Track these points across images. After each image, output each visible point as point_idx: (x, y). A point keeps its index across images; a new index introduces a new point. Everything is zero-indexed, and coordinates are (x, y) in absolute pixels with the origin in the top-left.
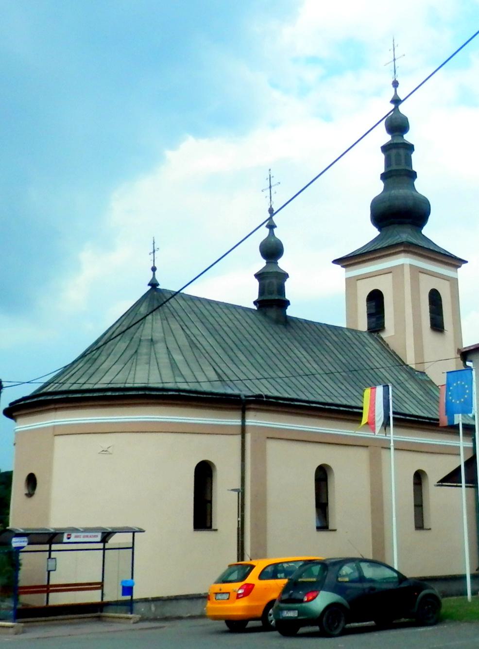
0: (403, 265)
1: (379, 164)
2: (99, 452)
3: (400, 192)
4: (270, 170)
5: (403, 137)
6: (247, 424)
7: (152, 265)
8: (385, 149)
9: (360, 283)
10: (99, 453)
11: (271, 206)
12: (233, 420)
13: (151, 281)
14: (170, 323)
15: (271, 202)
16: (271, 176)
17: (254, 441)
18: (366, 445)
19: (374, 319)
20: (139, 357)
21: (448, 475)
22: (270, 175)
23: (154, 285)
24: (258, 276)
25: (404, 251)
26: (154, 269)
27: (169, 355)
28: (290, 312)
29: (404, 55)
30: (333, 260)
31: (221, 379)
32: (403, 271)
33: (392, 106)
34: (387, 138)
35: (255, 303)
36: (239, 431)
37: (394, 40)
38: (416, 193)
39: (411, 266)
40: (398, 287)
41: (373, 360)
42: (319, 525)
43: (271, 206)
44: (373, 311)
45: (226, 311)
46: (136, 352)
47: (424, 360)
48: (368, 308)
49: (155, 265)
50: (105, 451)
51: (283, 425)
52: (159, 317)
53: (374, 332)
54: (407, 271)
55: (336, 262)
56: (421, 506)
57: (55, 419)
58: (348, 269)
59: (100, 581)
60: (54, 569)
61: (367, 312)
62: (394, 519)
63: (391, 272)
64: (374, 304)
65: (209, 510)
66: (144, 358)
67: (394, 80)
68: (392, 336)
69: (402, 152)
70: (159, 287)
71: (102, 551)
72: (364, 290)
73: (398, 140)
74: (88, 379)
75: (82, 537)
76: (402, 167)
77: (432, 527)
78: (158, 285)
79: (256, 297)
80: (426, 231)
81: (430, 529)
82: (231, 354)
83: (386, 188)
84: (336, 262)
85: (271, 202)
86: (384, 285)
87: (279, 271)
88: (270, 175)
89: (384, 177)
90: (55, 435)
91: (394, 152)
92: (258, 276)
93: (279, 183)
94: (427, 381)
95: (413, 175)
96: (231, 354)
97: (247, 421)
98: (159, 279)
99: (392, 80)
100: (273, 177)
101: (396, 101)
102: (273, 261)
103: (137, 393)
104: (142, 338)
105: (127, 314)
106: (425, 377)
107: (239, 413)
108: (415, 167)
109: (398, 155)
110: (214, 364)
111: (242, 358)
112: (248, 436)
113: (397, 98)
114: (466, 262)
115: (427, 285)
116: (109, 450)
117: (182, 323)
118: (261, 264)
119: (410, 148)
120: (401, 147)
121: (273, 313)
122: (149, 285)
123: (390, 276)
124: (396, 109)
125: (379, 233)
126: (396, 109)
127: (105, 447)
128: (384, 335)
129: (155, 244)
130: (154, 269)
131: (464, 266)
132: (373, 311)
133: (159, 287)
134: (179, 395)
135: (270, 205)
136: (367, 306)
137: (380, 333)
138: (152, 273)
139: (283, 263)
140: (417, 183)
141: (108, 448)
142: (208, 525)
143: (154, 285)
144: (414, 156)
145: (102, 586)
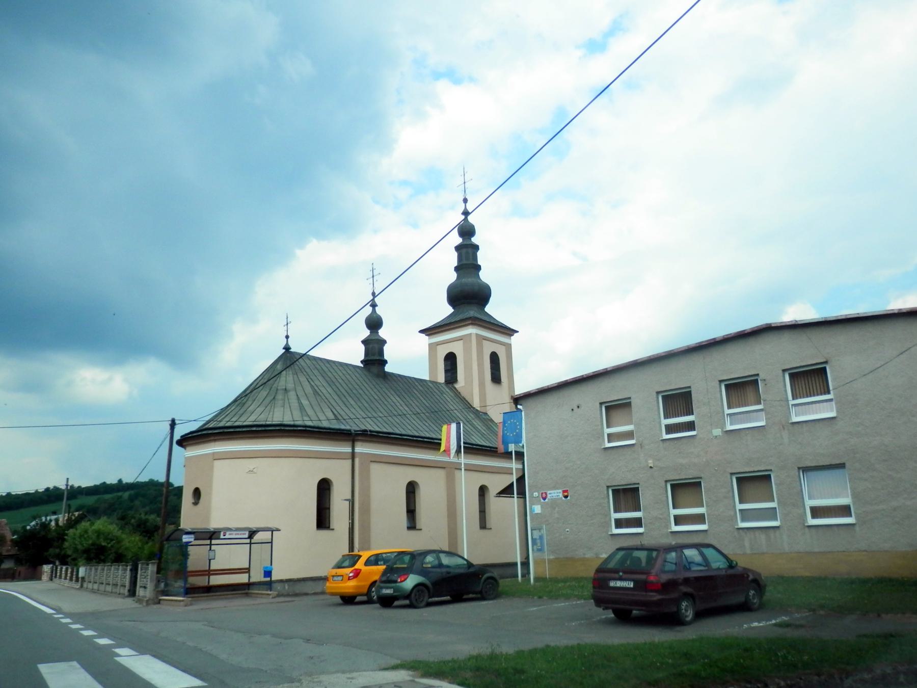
0: (471, 334)
7: (286, 334)
12: (346, 449)
14: (299, 377)
19: (449, 374)
23: (287, 348)
24: (364, 342)
25: (472, 324)
26: (287, 337)
28: (388, 368)
29: (472, 179)
33: (463, 217)
36: (350, 456)
38: (480, 281)
44: (449, 368)
46: (274, 398)
48: (446, 366)
53: (450, 383)
55: (422, 331)
59: (248, 567)
63: (462, 339)
66: (280, 402)
69: (470, 250)
70: (291, 350)
71: (249, 545)
72: (442, 352)
76: (471, 262)
77: (492, 528)
78: (290, 349)
79: (362, 357)
80: (488, 309)
81: (491, 529)
82: (344, 399)
84: (422, 331)
89: (457, 269)
90: (215, 460)
91: (464, 251)
92: (364, 342)
95: (478, 268)
96: (344, 399)
99: (462, 198)
101: (466, 213)
107: (350, 443)
108: (479, 263)
109: (467, 253)
111: (352, 402)
112: (357, 460)
115: (488, 348)
119: (476, 248)
121: (375, 369)
122: (284, 348)
124: (466, 219)
125: (453, 310)
127: (251, 468)
130: (287, 337)
131: (515, 334)
132: (449, 368)
133: (291, 350)
136: (444, 364)
138: (286, 340)
139: (382, 333)
141: (254, 469)
142: (327, 526)
143: (287, 348)
144: (479, 254)
145: (249, 570)
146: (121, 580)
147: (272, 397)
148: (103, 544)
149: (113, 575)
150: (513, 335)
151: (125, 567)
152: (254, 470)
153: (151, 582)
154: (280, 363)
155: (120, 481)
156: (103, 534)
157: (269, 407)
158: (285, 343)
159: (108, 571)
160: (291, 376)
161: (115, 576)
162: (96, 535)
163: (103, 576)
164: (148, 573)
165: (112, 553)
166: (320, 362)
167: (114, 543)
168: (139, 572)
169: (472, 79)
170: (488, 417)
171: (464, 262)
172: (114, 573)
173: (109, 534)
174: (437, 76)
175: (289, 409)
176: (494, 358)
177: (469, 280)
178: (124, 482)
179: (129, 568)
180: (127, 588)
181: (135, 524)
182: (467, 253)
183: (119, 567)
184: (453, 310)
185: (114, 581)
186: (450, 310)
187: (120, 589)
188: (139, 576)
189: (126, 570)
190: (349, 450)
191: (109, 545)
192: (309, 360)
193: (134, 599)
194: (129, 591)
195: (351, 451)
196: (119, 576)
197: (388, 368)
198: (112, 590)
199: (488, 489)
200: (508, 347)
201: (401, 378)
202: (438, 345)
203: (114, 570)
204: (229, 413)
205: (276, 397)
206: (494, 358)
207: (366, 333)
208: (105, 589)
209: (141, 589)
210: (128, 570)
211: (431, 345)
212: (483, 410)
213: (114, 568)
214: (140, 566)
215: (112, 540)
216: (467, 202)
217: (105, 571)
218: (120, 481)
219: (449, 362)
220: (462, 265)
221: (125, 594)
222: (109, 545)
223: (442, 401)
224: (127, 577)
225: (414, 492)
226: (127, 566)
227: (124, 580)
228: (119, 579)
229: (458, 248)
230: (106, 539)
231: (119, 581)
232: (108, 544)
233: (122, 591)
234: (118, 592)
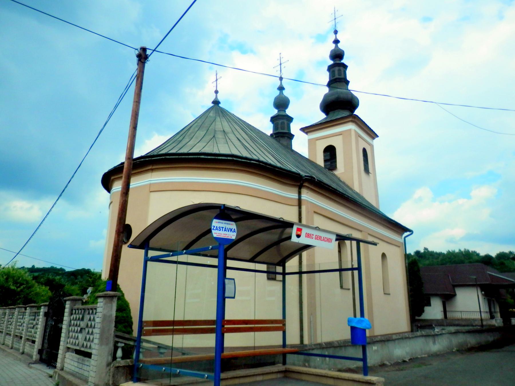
0: (350, 130)
1: (326, 78)
3: (340, 91)
5: (285, 111)
6: (302, 198)
7: (215, 89)
9: (318, 142)
12: (292, 194)
13: (215, 99)
15: (281, 73)
17: (308, 212)
18: (361, 229)
19: (329, 163)
22: (280, 57)
23: (216, 102)
25: (352, 121)
26: (216, 92)
29: (342, 15)
30: (300, 128)
32: (351, 133)
34: (275, 112)
36: (296, 203)
37: (335, 8)
39: (355, 131)
40: (347, 143)
44: (328, 158)
46: (214, 136)
48: (325, 156)
49: (218, 89)
51: (321, 204)
54: (353, 133)
57: (151, 178)
59: (280, 317)
60: (233, 296)
61: (324, 159)
62: (493, 274)
63: (341, 134)
64: (329, 154)
67: (335, 29)
68: (342, 173)
70: (220, 105)
71: (297, 276)
72: (322, 146)
73: (282, 113)
74: (179, 150)
75: (314, 237)
76: (342, 76)
77: (391, 293)
81: (389, 294)
83: (330, 91)
85: (281, 73)
86: (337, 143)
88: (280, 57)
90: (151, 192)
95: (347, 82)
97: (302, 195)
98: (220, 98)
99: (333, 31)
100: (283, 58)
101: (336, 42)
102: (283, 109)
103: (226, 158)
104: (216, 130)
105: (199, 118)
107: (296, 190)
109: (339, 70)
112: (304, 208)
113: (337, 39)
115: (362, 145)
120: (341, 66)
123: (341, 137)
124: (337, 46)
126: (337, 46)
128: (336, 173)
129: (217, 75)
130: (216, 92)
132: (328, 158)
134: (259, 164)
136: (323, 155)
138: (215, 94)
139: (289, 112)
140: (350, 87)
143: (216, 102)
144: (348, 72)
145: (284, 325)
146: (27, 331)
147: (212, 136)
148: (13, 287)
149: (17, 322)
151: (35, 310)
153: (101, 343)
154: (212, 112)
155: (33, 266)
156: (13, 277)
159: (11, 317)
161: (18, 324)
162: (5, 277)
163: (3, 323)
164: (38, 320)
165: (20, 298)
167: (24, 288)
168: (66, 318)
169: (252, 51)
172: (17, 319)
173: (19, 279)
174: (232, 48)
176: (364, 151)
178: (36, 267)
179: (43, 310)
180: (38, 345)
181: (44, 282)
182: (339, 70)
183: (26, 309)
185: (17, 331)
187: (24, 345)
188: (64, 326)
189: (36, 314)
190: (295, 196)
191: (19, 289)
193: (51, 371)
194: (40, 352)
195: (297, 197)
196: (25, 325)
198: (12, 343)
200: (372, 146)
202: (317, 140)
203: (18, 315)
204: (165, 148)
206: (364, 151)
208: (4, 340)
209: (69, 355)
210: (41, 314)
211: (310, 141)
213: (19, 312)
214: (68, 305)
215: (22, 284)
217: (7, 316)
218: (33, 266)
221: (31, 356)
222: (19, 289)
224: (39, 326)
226: (39, 308)
227: (33, 331)
228: (25, 328)
230: (15, 282)
231: (24, 333)
232: (18, 287)
233: (27, 349)
234: (21, 351)
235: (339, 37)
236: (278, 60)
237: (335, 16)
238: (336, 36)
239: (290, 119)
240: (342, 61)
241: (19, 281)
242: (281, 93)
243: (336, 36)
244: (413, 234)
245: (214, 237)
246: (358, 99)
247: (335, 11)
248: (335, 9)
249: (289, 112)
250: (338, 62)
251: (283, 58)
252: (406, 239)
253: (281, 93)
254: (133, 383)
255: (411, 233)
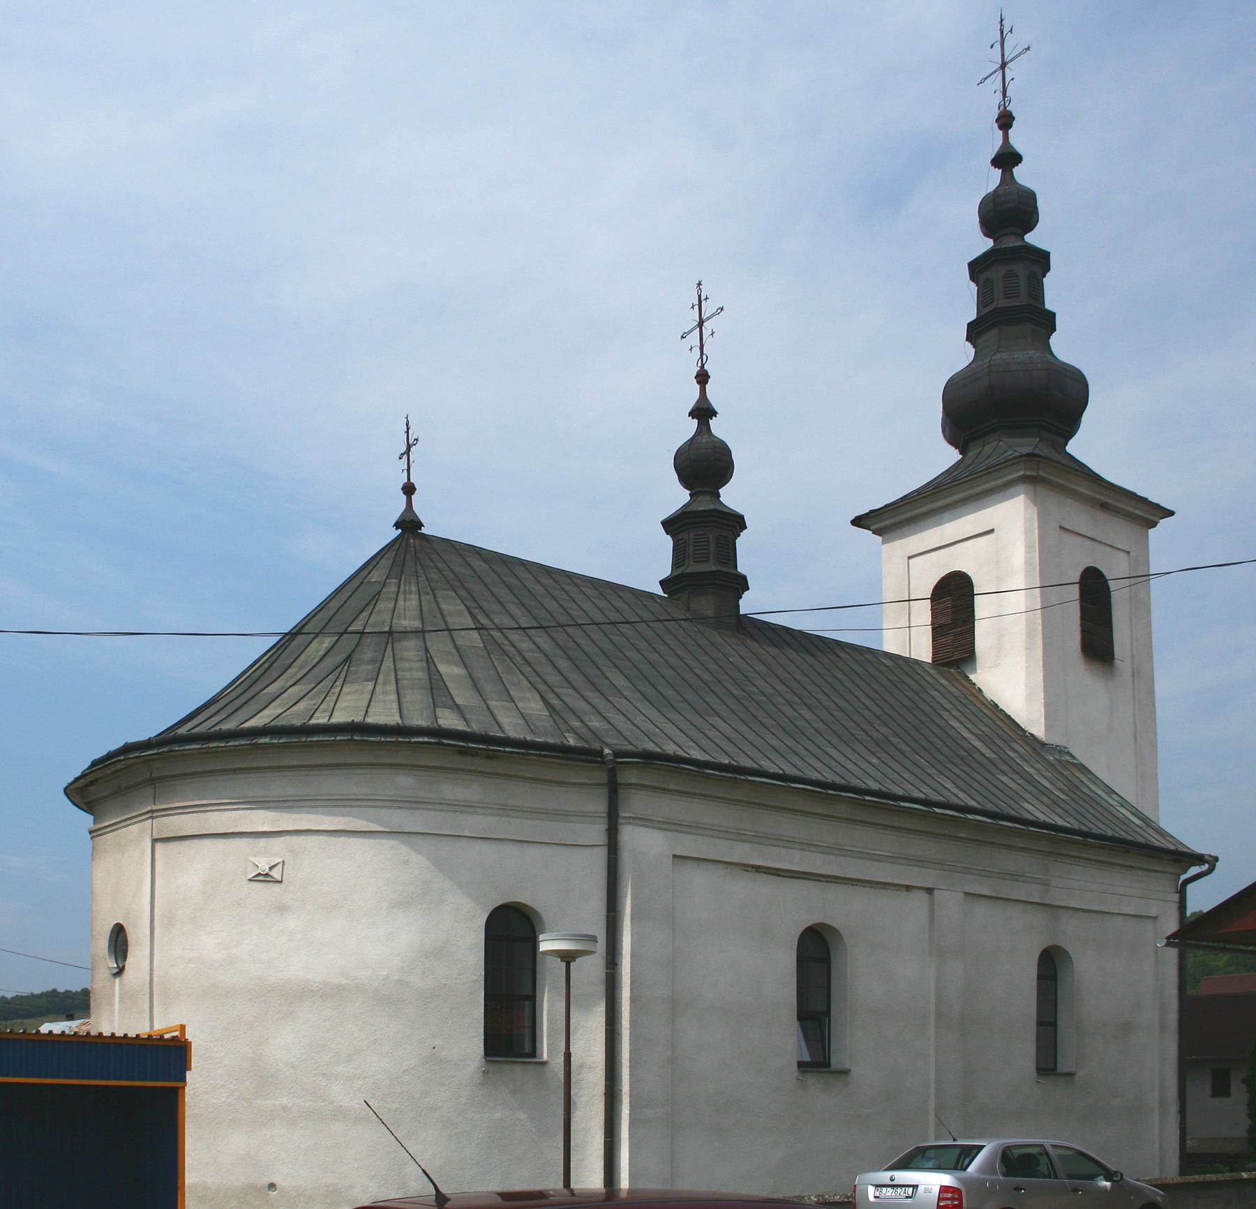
2: (251, 876)
4: (699, 284)
5: (1024, 239)
8: (977, 268)
10: (250, 880)
11: (703, 366)
14: (440, 600)
16: (703, 297)
20: (352, 669)
21: (1217, 907)
23: (409, 524)
24: (670, 525)
27: (428, 663)
28: (748, 604)
29: (1028, 49)
31: (478, 626)
33: (997, 174)
35: (663, 583)
37: (1002, 20)
38: (1049, 357)
41: (946, 715)
42: (807, 1058)
43: (703, 366)
44: (946, 620)
45: (589, 592)
47: (1149, 572)
50: (264, 878)
52: (414, 588)
53: (949, 664)
55: (858, 522)
56: (1054, 1025)
58: (886, 536)
65: (527, 1021)
66: (365, 669)
69: (1020, 269)
70: (424, 530)
78: (420, 525)
79: (666, 571)
80: (1073, 447)
82: (591, 671)
84: (858, 522)
87: (720, 508)
89: (975, 332)
91: (997, 273)
92: (670, 525)
93: (722, 309)
94: (1072, 764)
95: (1047, 322)
96: (591, 671)
99: (995, 113)
106: (1068, 758)
110: (542, 687)
111: (620, 682)
114: (1171, 513)
116: (276, 874)
117: (470, 603)
118: (678, 497)
119: (1041, 260)
121: (706, 605)
122: (397, 525)
125: (1001, 170)
126: (1007, 177)
127: (264, 867)
131: (1163, 523)
133: (424, 530)
135: (700, 364)
137: (963, 668)
139: (730, 496)
140: (1054, 341)
141: (271, 868)
142: (527, 1049)
143: (409, 524)
144: (1050, 283)
147: (345, 656)
150: (1154, 525)
152: (272, 873)
157: (327, 683)
158: (403, 506)
160: (415, 596)
166: (520, 572)
170: (1068, 758)
171: (1002, 303)
175: (392, 687)
177: (1021, 355)
184: (1001, 170)
186: (952, 456)
192: (485, 561)
197: (748, 604)
199: (1072, 962)
201: (792, 636)
205: (356, 656)
207: (678, 497)
212: (1056, 740)
216: (1010, 126)
219: (949, 603)
220: (997, 312)
223: (922, 706)
225: (826, 961)
229: (977, 268)
235: (1017, 139)
236: (693, 307)
237: (1003, 55)
238: (1006, 137)
239: (737, 523)
240: (1031, 238)
241: (548, 714)
242: (704, 428)
243: (1006, 137)
244: (1214, 873)
245: (92, 815)
246: (1087, 386)
247: (1002, 32)
248: (1002, 25)
249: (730, 496)
250: (1011, 242)
251: (707, 298)
252: (1190, 887)
253: (704, 427)
254: (190, 1070)
255: (1206, 867)
